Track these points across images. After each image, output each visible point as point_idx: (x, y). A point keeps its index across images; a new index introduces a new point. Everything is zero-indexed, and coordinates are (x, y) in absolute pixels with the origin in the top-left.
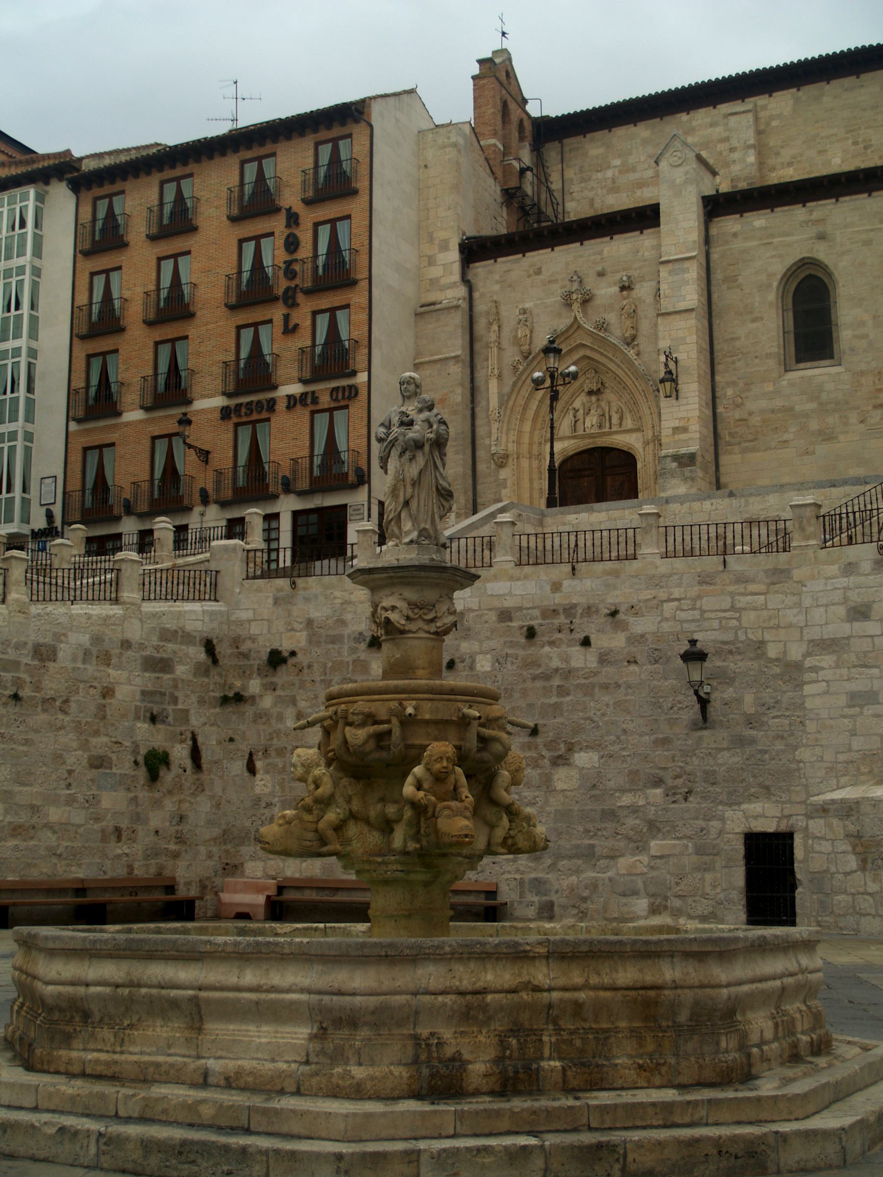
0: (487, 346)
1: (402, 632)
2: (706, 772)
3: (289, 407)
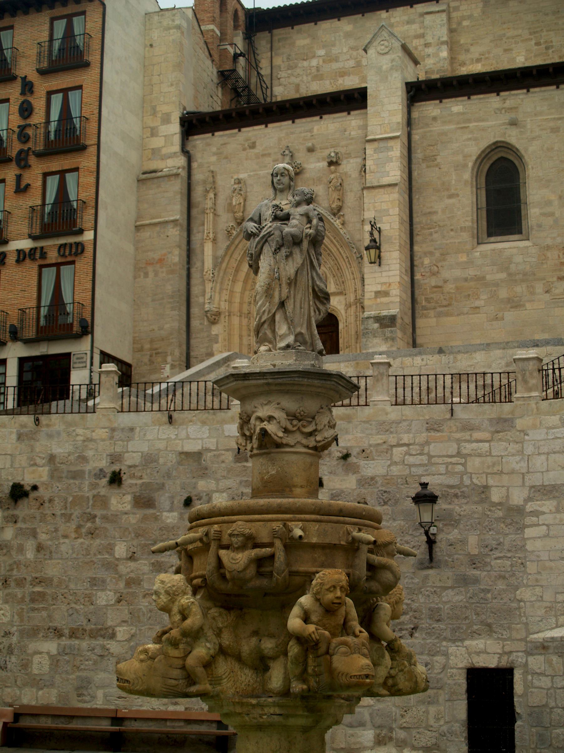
0: (204, 212)
1: (279, 445)
2: (431, 609)
3: (18, 261)
